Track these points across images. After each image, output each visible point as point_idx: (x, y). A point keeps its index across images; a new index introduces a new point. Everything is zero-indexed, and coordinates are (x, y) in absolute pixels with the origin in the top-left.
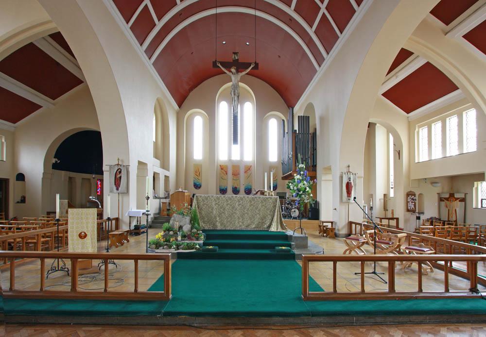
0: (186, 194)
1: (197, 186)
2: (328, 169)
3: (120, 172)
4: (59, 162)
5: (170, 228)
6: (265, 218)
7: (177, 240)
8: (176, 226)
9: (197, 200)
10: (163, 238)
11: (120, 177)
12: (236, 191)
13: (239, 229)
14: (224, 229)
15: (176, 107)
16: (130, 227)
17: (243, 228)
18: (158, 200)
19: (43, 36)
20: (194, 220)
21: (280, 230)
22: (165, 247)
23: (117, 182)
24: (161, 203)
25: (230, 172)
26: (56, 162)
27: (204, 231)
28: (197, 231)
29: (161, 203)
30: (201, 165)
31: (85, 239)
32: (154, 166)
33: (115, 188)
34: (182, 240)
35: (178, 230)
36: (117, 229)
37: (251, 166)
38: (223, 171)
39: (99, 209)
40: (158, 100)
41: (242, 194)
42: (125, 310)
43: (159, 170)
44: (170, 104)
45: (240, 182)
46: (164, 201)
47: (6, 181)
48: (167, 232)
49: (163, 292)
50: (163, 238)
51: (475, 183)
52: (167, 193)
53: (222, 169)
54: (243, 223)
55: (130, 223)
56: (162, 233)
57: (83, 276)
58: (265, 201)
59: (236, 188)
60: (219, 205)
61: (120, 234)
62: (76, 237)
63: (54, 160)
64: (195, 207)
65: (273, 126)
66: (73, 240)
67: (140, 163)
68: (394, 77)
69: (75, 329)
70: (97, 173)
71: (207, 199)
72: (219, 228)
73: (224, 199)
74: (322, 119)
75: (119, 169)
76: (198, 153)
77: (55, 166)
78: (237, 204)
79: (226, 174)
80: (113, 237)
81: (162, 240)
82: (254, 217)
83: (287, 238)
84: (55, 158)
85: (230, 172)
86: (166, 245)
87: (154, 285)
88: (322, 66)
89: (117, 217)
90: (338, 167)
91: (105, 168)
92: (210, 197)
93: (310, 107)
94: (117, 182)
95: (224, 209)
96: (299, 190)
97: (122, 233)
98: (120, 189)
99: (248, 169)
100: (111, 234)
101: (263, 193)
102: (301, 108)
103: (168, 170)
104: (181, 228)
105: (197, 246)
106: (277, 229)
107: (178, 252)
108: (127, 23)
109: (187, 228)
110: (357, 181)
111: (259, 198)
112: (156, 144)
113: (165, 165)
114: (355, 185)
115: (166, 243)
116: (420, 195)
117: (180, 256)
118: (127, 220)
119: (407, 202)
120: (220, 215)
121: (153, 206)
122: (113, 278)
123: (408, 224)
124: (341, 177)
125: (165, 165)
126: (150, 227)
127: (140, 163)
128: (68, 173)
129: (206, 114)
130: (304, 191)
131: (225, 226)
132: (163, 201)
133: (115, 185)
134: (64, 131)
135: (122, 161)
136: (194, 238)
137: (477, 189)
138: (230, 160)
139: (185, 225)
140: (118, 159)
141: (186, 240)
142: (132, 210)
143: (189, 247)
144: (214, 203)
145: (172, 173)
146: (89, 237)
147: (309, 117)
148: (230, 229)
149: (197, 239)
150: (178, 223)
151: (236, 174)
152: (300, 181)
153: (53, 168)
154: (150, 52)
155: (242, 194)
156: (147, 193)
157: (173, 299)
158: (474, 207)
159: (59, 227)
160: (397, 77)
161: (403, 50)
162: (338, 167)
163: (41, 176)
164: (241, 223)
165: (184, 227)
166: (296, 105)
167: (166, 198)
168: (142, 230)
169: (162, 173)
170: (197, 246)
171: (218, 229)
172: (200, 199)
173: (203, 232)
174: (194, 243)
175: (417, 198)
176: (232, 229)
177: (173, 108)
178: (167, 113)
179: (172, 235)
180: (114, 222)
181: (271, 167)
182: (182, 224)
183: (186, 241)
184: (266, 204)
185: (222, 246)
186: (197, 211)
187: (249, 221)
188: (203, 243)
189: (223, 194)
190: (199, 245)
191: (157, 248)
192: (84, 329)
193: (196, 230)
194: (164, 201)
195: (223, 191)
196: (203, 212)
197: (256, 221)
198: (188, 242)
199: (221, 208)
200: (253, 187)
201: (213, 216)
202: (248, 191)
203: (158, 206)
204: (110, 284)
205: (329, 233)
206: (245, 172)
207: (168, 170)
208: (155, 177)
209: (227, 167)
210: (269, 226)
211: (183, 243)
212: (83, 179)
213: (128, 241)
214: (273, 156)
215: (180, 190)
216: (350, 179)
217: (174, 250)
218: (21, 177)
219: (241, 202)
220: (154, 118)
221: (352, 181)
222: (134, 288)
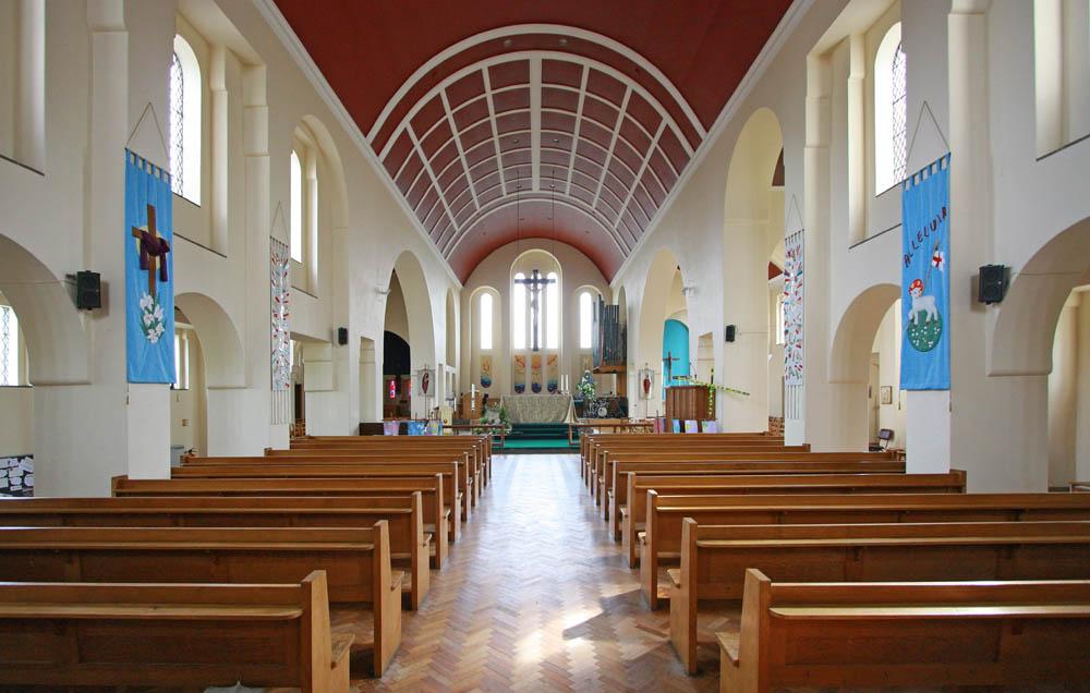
1: (486, 384)
2: (633, 369)
12: (536, 388)
20: (502, 416)
23: (425, 385)
25: (529, 363)
33: (422, 391)
41: (545, 393)
76: (486, 342)
94: (425, 385)
99: (553, 359)
108: (378, 154)
109: (497, 421)
120: (523, 411)
124: (639, 375)
151: (536, 366)
154: (378, 146)
155: (545, 393)
159: (615, 375)
161: (783, 184)
181: (583, 354)
195: (519, 389)
206: (549, 364)
208: (447, 373)
209: (524, 357)
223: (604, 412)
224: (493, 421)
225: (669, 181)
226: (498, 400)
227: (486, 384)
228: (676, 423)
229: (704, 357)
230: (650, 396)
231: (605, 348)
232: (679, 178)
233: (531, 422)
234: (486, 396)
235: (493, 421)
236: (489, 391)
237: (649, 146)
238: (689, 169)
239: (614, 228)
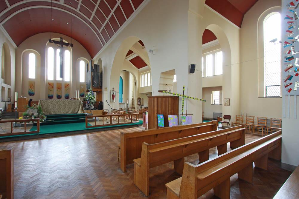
0: (26, 99)
6: (76, 109)
12: (59, 97)
15: (15, 46)
17: (65, 113)
18: (4, 103)
20: (39, 111)
21: (82, 113)
25: (55, 87)
30: (35, 82)
37: (69, 84)
41: (63, 99)
44: (11, 44)
45: (62, 92)
51: (212, 92)
53: (50, 85)
54: (65, 111)
58: (76, 102)
59: (59, 95)
65: (82, 64)
68: (131, 56)
71: (46, 101)
74: (105, 68)
76: (32, 74)
79: (53, 87)
82: (70, 108)
83: (85, 115)
85: (55, 87)
88: (107, 43)
90: (109, 89)
93: (100, 61)
95: (55, 106)
96: (89, 98)
99: (67, 85)
101: (75, 99)
102: (96, 59)
105: (43, 121)
106: (81, 112)
109: (36, 114)
110: (117, 94)
111: (73, 101)
114: (116, 95)
116: (142, 99)
119: (138, 102)
123: (138, 109)
124: (110, 92)
130: (92, 98)
137: (213, 94)
144: (50, 103)
145: (12, 87)
147: (99, 65)
149: (43, 118)
152: (90, 95)
155: (63, 99)
158: (211, 104)
160: (132, 56)
162: (109, 89)
166: (95, 57)
167: (8, 102)
170: (43, 121)
175: (141, 100)
181: (82, 84)
182: (33, 113)
185: (55, 120)
187: (68, 111)
189: (50, 99)
190: (44, 120)
195: (51, 97)
197: (72, 110)
199: (60, 105)
200: (70, 96)
201: (49, 109)
202: (67, 97)
205: (104, 114)
206: (65, 87)
209: (53, 84)
210: (77, 112)
214: (82, 79)
216: (114, 93)
221: (114, 94)
223: (93, 107)
224: (33, 114)
225: (116, 28)
226: (37, 103)
227: (31, 94)
228: (161, 118)
229: (162, 83)
230: (114, 101)
231: (93, 81)
232: (127, 20)
233: (58, 113)
234: (31, 100)
235: (33, 114)
236: (34, 98)
237: (102, 27)
238: (119, 31)
239: (100, 32)
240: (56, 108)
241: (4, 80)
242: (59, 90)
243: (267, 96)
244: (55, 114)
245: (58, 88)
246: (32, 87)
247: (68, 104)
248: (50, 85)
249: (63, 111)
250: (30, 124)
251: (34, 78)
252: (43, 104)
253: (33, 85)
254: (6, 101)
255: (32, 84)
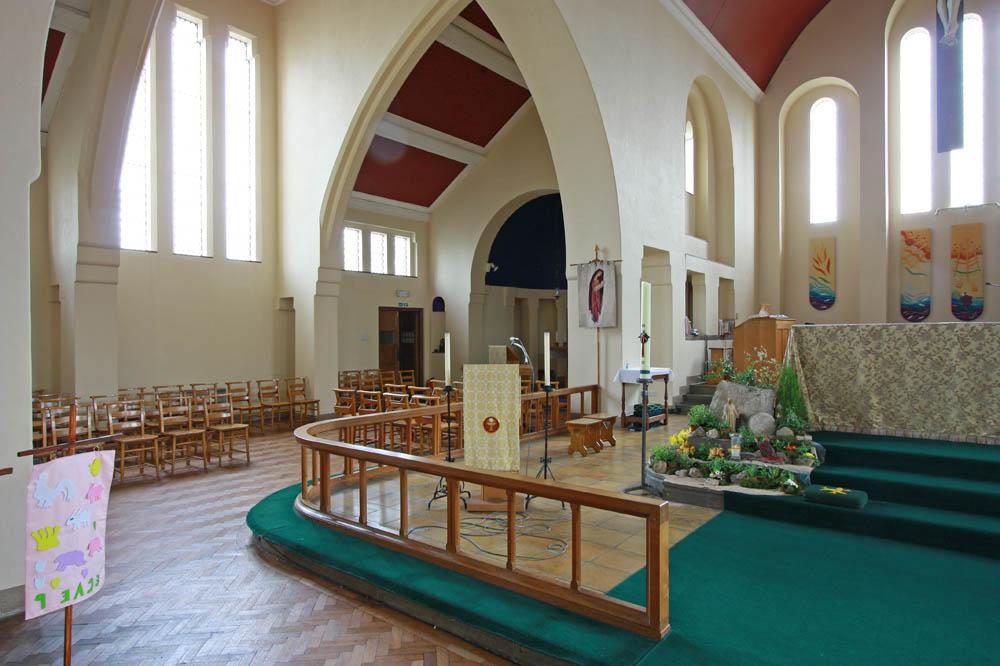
0: (779, 325)
1: (821, 302)
3: (601, 279)
4: (496, 269)
5: (709, 418)
7: (727, 455)
8: (730, 414)
9: (800, 343)
10: (689, 446)
11: (601, 290)
13: (962, 438)
14: (900, 433)
15: (752, 89)
16: (623, 408)
18: (701, 343)
19: (451, 21)
20: (786, 399)
22: (693, 470)
24: (709, 351)
25: (942, 250)
26: (492, 269)
27: (819, 435)
28: (796, 434)
29: (709, 351)
30: (835, 240)
31: (497, 432)
32: (687, 254)
33: (590, 317)
34: (743, 457)
35: (733, 425)
36: (596, 412)
38: (914, 248)
39: (524, 366)
40: (697, 83)
42: (536, 632)
43: (700, 265)
44: (732, 85)
46: (718, 344)
47: (419, 312)
48: (700, 430)
49: (643, 609)
50: (689, 446)
52: (727, 325)
53: (909, 242)
54: (982, 418)
55: (623, 400)
56: (687, 433)
57: (490, 516)
59: (967, 299)
60: (878, 356)
61: (591, 426)
62: (479, 428)
63: (488, 267)
64: (793, 361)
66: (472, 433)
67: (649, 251)
69: (435, 643)
70: (561, 288)
72: (879, 426)
73: (898, 335)
75: (599, 270)
76: (824, 205)
77: (491, 279)
78: (903, 351)
79: (928, 256)
80: (575, 431)
81: (686, 450)
84: (489, 262)
86: (696, 465)
87: (634, 576)
89: (596, 383)
91: (570, 272)
92: (847, 330)
95: (900, 369)
97: (597, 423)
98: (600, 317)
100: (572, 425)
103: (731, 263)
104: (742, 420)
105: (791, 482)
107: (726, 492)
109: (760, 423)
112: (694, 200)
113: (721, 252)
115: (694, 460)
117: (732, 502)
118: (616, 391)
121: (684, 360)
122: (547, 535)
125: (721, 252)
126: (672, 412)
127: (649, 251)
128: (513, 289)
129: (854, 89)
131: (903, 426)
132: (712, 344)
133: (590, 309)
134: (507, 201)
135: (605, 251)
136: (781, 454)
138: (942, 210)
139: (757, 412)
140: (597, 249)
141: (757, 458)
142: (629, 369)
143: (762, 481)
144: (859, 349)
145: (742, 271)
146: (502, 429)
148: (925, 435)
149: (793, 460)
150: (733, 407)
153: (486, 283)
156: (644, 326)
157: (673, 639)
163: (468, 300)
164: (973, 421)
165: (752, 421)
167: (723, 337)
168: (652, 419)
169: (712, 273)
170: (791, 482)
171: (875, 432)
172: (810, 337)
173: (814, 440)
174: (781, 470)
176: (934, 436)
177: (745, 95)
178: (726, 113)
179: (713, 441)
180: (588, 395)
182: (745, 410)
183: (755, 462)
184: (878, 347)
185: (876, 491)
186: (801, 374)
188: (812, 472)
190: (798, 478)
191: (671, 471)
192: (452, 648)
193: (791, 433)
194: (718, 344)
195: (915, 312)
196: (820, 380)
198: (760, 464)
199: (938, 365)
203: (700, 356)
204: (519, 550)
207: (731, 263)
208: (692, 283)
209: (930, 233)
211: (744, 465)
212: (541, 300)
213: (613, 443)
215: (763, 314)
217: (716, 482)
218: (439, 304)
219: (830, 345)
220: (689, 134)
222: (571, 580)
240: (902, 384)
241: (709, 245)
242: (962, 268)
243: (579, 394)
244: (894, 430)
245: (958, 255)
246: (823, 267)
247: (954, 352)
248: (909, 242)
249: (962, 417)
250: (704, 491)
251: (812, 222)
252: (815, 350)
253: (830, 255)
254: (708, 333)
255: (824, 252)
